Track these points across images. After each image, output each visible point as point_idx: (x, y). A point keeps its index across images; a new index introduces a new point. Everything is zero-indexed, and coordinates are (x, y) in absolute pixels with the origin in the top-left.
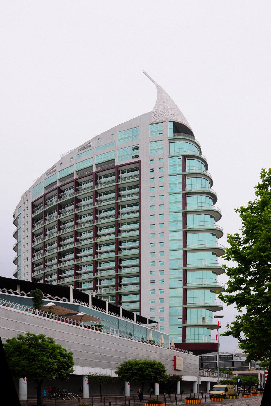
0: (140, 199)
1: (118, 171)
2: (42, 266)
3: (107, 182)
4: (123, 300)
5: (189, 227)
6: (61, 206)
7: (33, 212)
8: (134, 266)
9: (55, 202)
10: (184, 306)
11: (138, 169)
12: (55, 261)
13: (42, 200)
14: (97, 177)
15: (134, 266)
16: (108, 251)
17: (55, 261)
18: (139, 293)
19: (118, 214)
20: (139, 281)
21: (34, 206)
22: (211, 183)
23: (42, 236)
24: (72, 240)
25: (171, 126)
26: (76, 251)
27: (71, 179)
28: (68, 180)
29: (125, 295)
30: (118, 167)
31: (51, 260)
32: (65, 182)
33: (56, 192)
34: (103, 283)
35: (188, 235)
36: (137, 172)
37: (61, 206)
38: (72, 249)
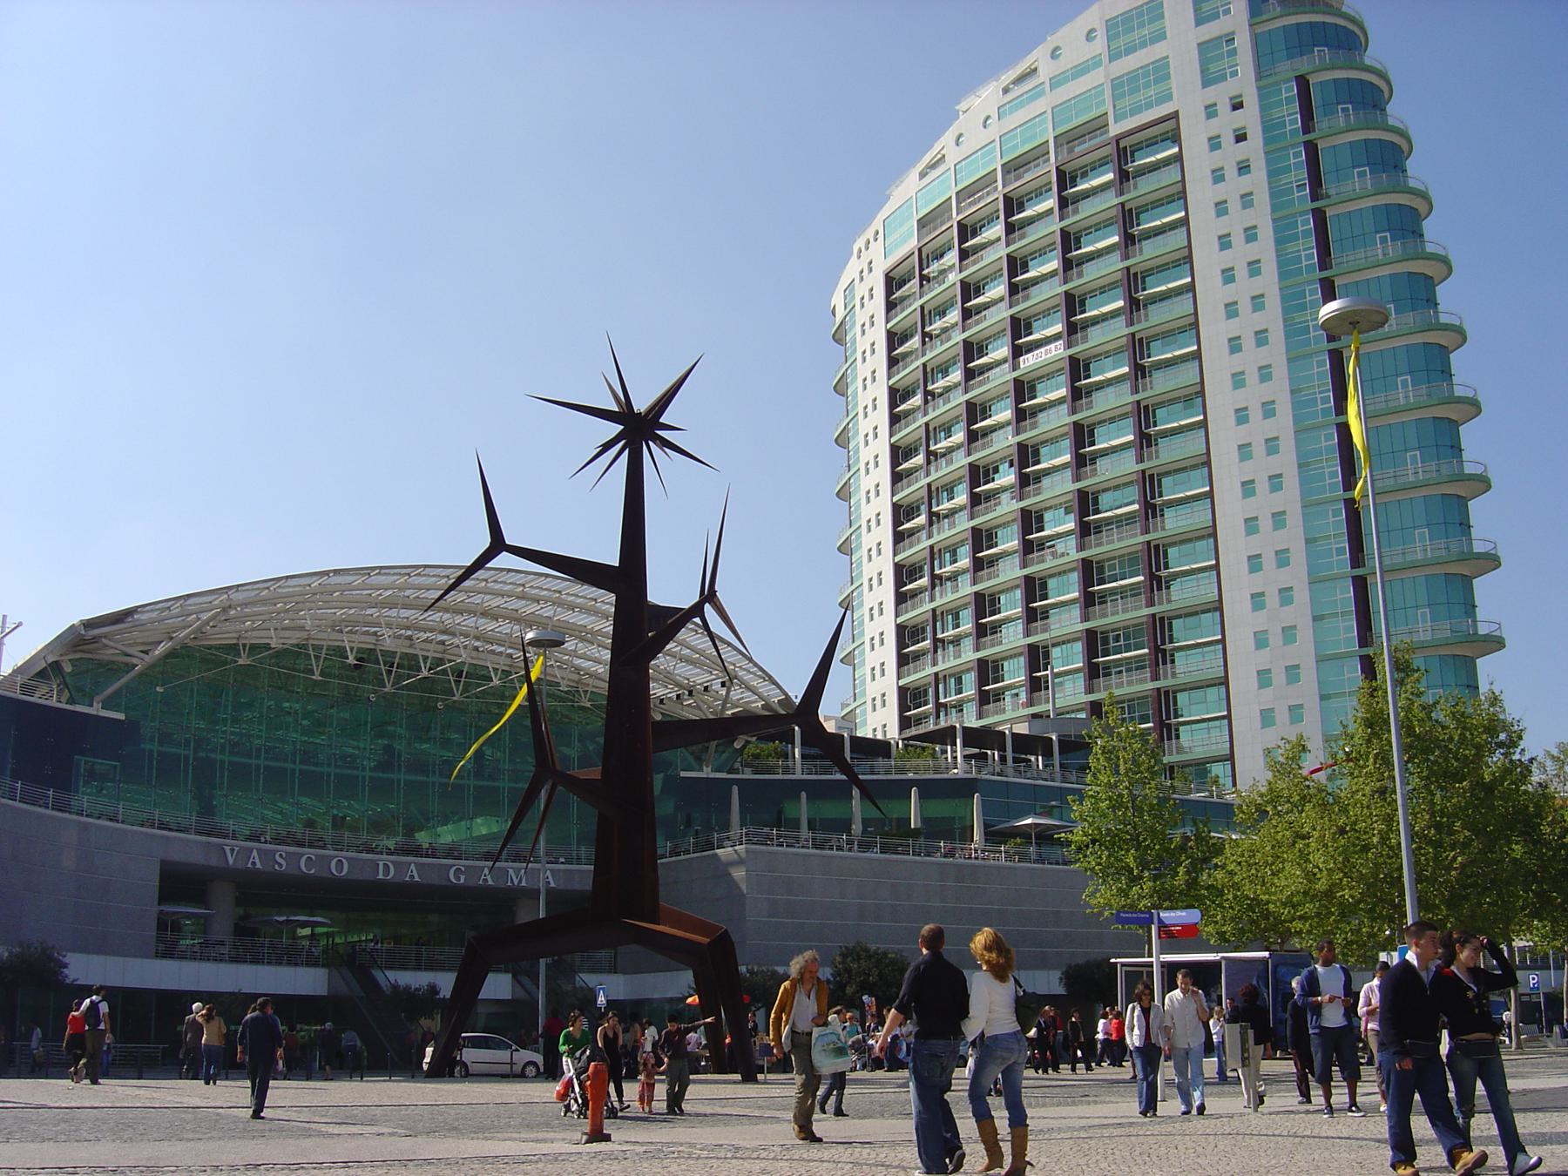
11: (1175, 138)
12: (959, 436)
20: (1214, 596)
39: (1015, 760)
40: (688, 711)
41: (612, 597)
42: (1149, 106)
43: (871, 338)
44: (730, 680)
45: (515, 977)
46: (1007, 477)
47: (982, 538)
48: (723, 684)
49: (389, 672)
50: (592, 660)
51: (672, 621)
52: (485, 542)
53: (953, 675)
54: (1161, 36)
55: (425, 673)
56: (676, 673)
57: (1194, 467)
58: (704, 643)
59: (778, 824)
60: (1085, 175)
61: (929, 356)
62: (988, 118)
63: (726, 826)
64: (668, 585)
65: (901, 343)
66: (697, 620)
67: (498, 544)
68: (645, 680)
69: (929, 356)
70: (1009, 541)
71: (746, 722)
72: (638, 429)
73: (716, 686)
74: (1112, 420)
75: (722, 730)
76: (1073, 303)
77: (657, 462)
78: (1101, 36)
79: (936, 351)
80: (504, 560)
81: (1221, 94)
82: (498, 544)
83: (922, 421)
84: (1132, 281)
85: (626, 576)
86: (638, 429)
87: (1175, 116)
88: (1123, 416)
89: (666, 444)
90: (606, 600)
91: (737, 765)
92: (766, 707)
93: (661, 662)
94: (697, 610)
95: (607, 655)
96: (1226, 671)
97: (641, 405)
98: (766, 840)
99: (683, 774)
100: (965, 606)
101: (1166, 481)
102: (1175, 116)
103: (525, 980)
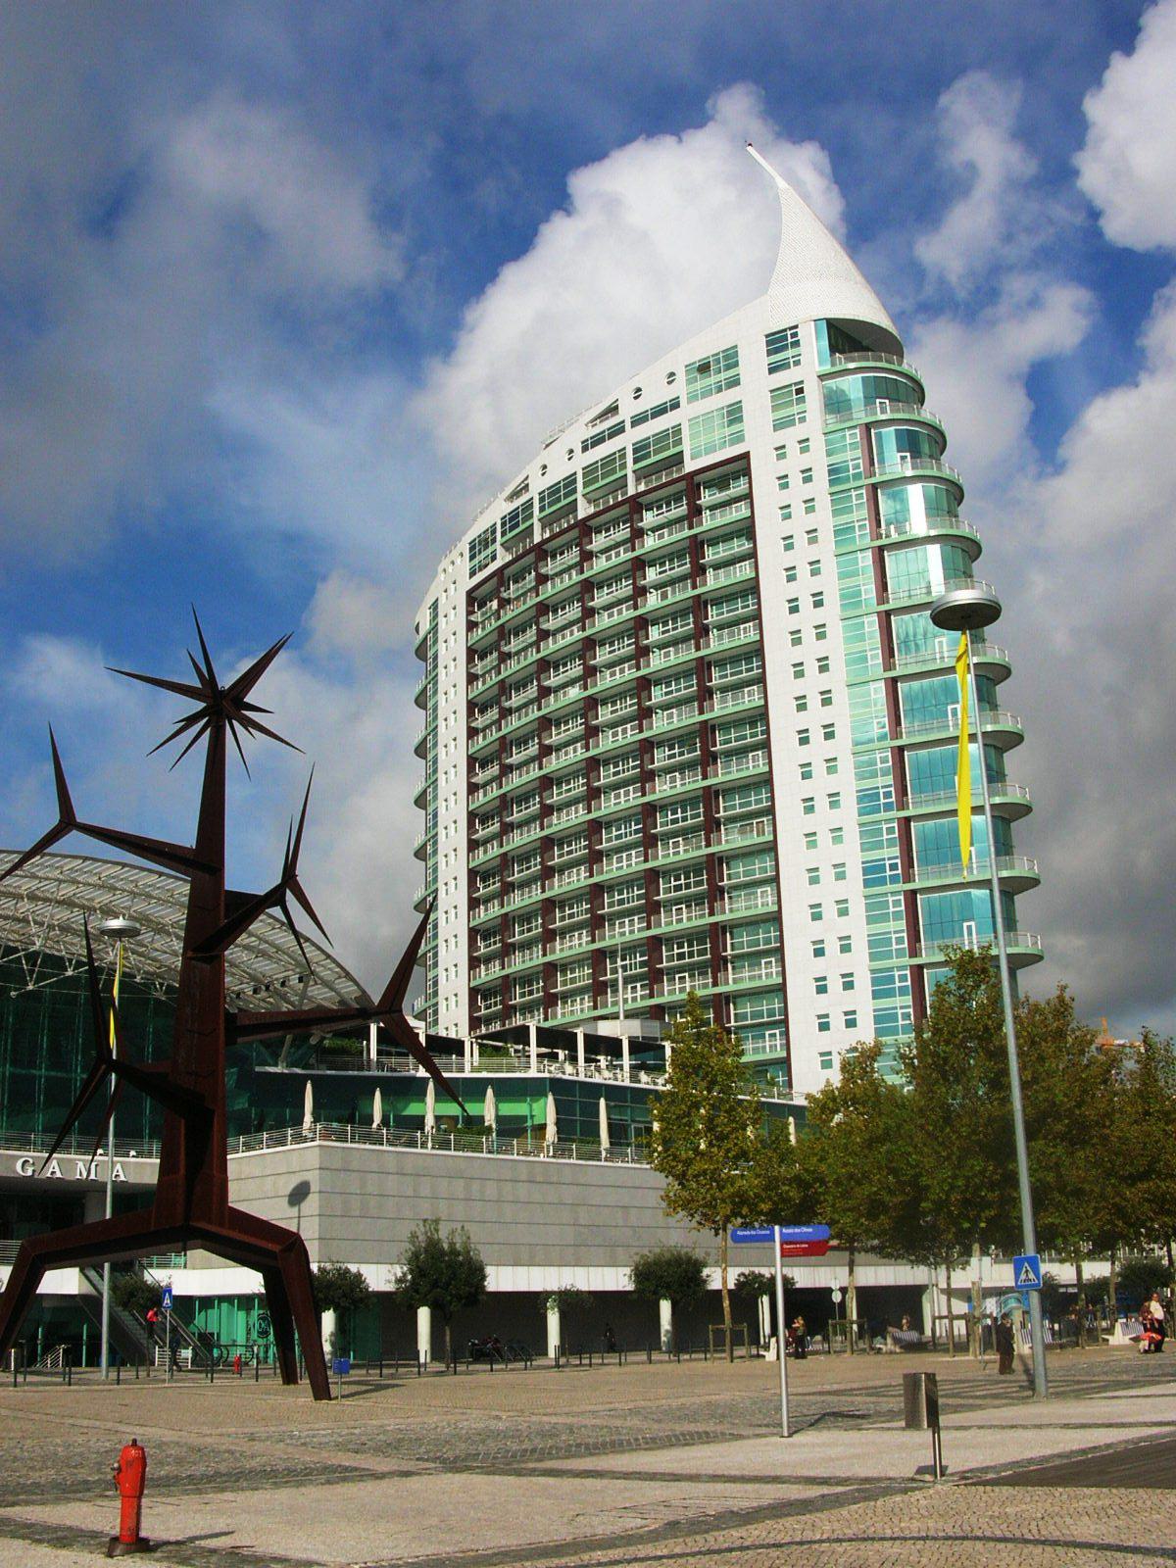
11: (747, 472)
39: (587, 1060)
40: (259, 1003)
41: (186, 888)
42: (723, 445)
43: (452, 650)
44: (307, 975)
45: (82, 1271)
48: (301, 980)
49: (31, 972)
50: (168, 952)
51: (248, 907)
52: (53, 819)
54: (734, 382)
55: (70, 973)
56: (253, 962)
58: (286, 939)
59: (351, 1120)
62: (571, 451)
63: (298, 1121)
64: (248, 868)
66: (276, 911)
67: (68, 822)
68: (219, 973)
71: (321, 1017)
73: (294, 981)
75: (301, 1023)
77: (242, 744)
78: (681, 377)
80: (73, 840)
81: (790, 436)
82: (68, 822)
85: (203, 860)
87: (746, 456)
89: (248, 723)
90: (181, 888)
91: (312, 1061)
92: (342, 1002)
93: (233, 953)
94: (276, 897)
95: (178, 946)
96: (784, 979)
97: (226, 680)
98: (342, 1137)
99: (258, 1069)
102: (746, 456)
103: (92, 1274)
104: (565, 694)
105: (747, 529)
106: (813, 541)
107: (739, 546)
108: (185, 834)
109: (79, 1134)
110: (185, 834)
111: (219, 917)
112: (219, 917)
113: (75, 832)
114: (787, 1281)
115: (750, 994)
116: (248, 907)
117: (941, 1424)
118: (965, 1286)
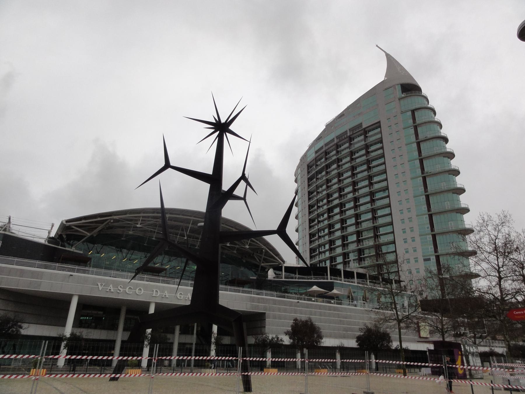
0: (384, 153)
1: (365, 132)
2: (315, 193)
3: (359, 142)
4: (377, 197)
5: (424, 154)
6: (328, 166)
7: (308, 172)
8: (381, 164)
9: (322, 163)
10: (437, 254)
11: (380, 127)
12: (324, 187)
13: (314, 161)
14: (351, 139)
15: (381, 164)
16: (362, 173)
17: (324, 187)
18: (391, 224)
19: (366, 137)
20: (385, 177)
21: (309, 167)
22: (435, 113)
23: (314, 167)
24: (334, 152)
25: (399, 88)
26: (339, 160)
27: (333, 143)
28: (331, 145)
29: (379, 209)
30: (365, 129)
31: (321, 186)
32: (329, 146)
33: (324, 154)
34: (362, 201)
35: (422, 145)
36: (379, 130)
37: (328, 166)
38: (335, 160)
46: (338, 226)
47: (331, 226)
52: (163, 164)
53: (323, 245)
56: (231, 211)
57: (386, 207)
60: (358, 152)
61: (318, 197)
65: (312, 208)
67: (168, 165)
69: (318, 197)
70: (339, 243)
72: (221, 128)
74: (366, 213)
76: (354, 184)
79: (320, 210)
82: (168, 165)
83: (316, 198)
84: (372, 194)
85: (214, 179)
86: (221, 128)
88: (371, 229)
90: (207, 186)
100: (326, 244)
101: (378, 211)
104: (347, 197)
105: (381, 141)
106: (412, 231)
107: (379, 145)
108: (209, 170)
109: (296, 358)
110: (209, 170)
111: (219, 196)
112: (219, 196)
113: (170, 169)
114: (350, 261)
115: (367, 230)
116: (230, 195)
117: (365, 252)
118: (423, 349)
